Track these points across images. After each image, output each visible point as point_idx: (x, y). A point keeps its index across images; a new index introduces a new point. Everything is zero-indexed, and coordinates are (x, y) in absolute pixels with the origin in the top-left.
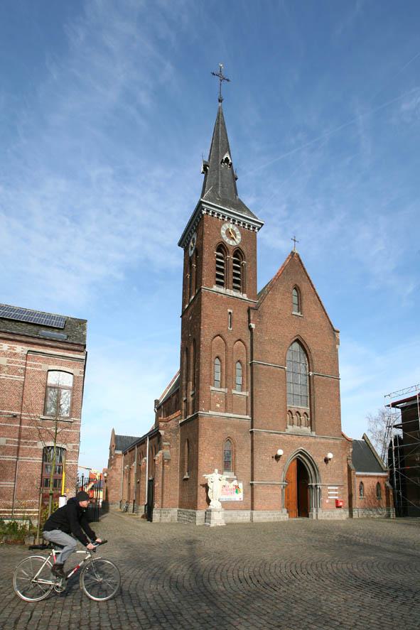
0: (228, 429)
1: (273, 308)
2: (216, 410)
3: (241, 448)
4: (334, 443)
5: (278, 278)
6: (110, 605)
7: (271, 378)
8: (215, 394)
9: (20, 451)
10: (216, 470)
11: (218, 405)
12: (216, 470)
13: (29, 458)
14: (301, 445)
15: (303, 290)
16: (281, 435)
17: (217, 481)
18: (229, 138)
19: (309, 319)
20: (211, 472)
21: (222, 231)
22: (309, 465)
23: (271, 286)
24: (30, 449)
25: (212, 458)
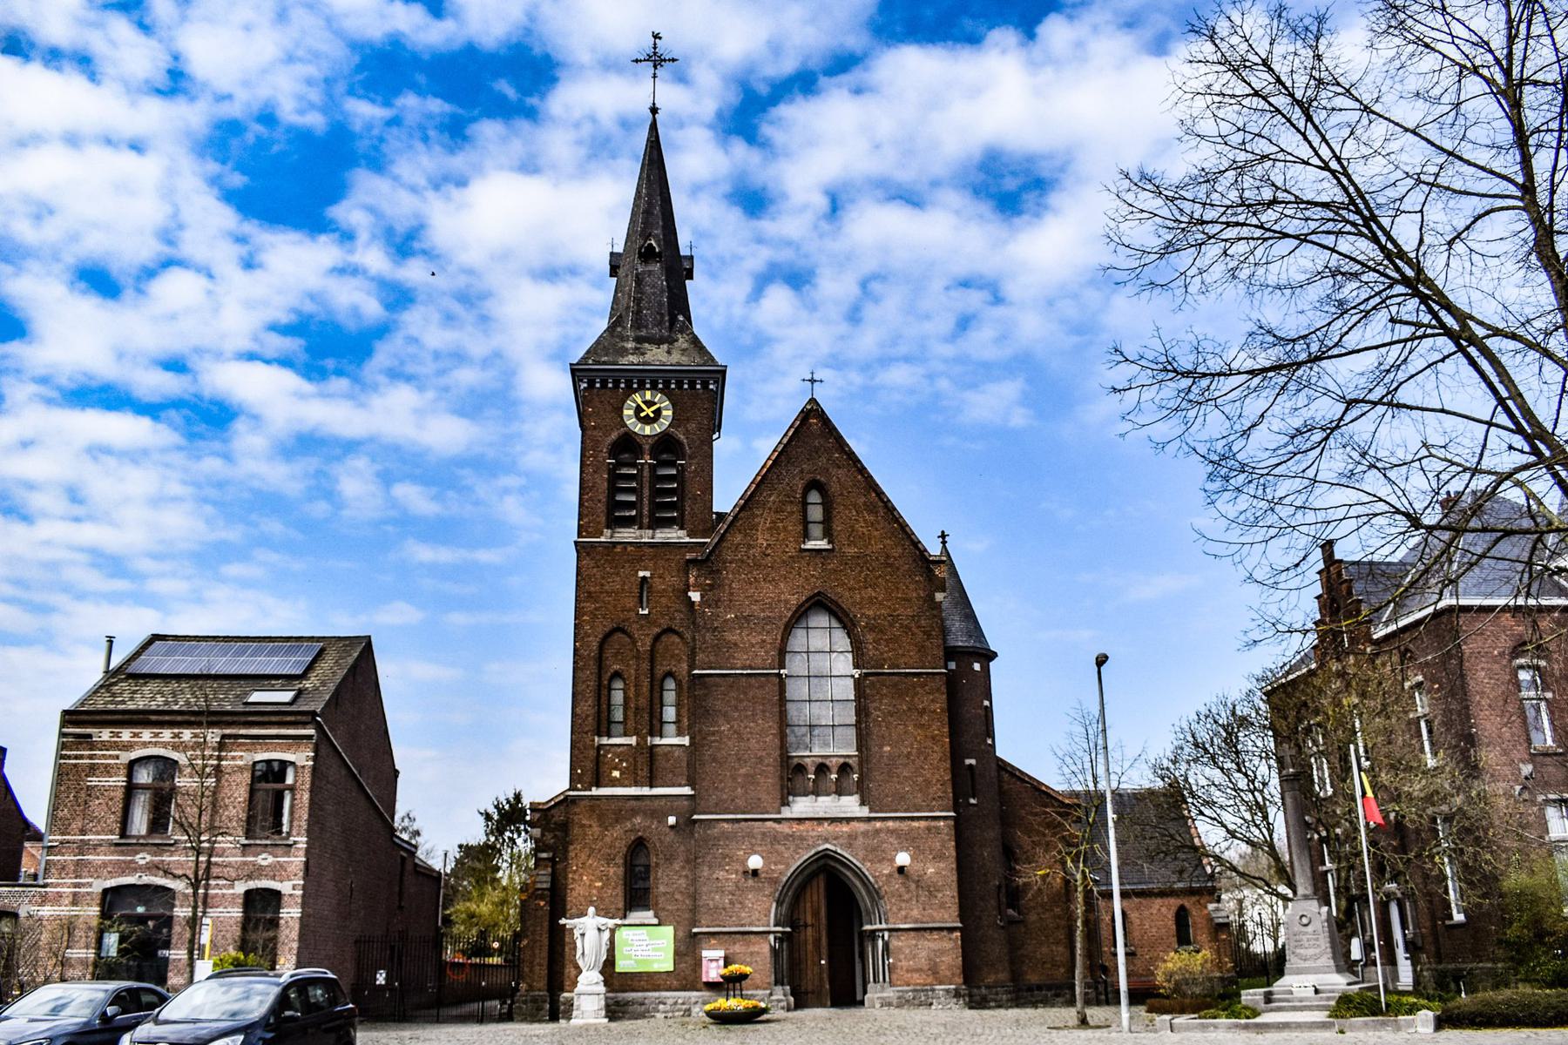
0: (638, 820)
1: (750, 547)
2: (614, 783)
3: (670, 859)
4: (929, 829)
5: (764, 481)
6: (1231, 904)
7: (741, 701)
8: (609, 752)
9: (209, 900)
10: (591, 910)
11: (616, 774)
12: (591, 910)
13: (221, 910)
14: (826, 840)
15: (834, 488)
16: (769, 824)
17: (591, 935)
18: (852, 443)
19: (852, 551)
20: (583, 914)
21: (626, 412)
22: (858, 883)
23: (749, 502)
24: (224, 895)
25: (599, 884)
